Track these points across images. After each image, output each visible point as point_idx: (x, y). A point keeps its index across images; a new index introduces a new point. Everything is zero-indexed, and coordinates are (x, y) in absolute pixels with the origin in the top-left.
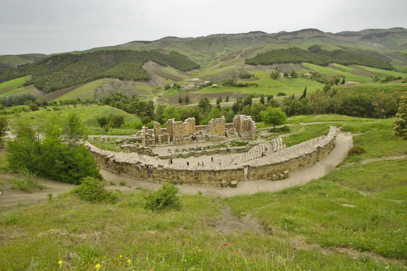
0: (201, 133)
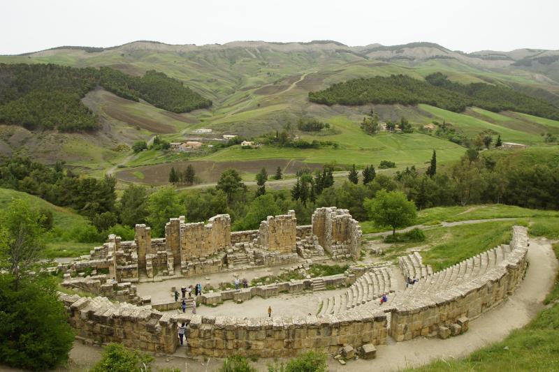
0: (243, 247)
